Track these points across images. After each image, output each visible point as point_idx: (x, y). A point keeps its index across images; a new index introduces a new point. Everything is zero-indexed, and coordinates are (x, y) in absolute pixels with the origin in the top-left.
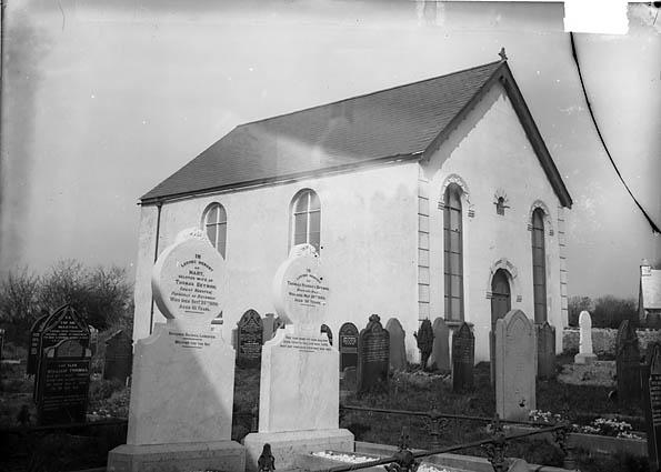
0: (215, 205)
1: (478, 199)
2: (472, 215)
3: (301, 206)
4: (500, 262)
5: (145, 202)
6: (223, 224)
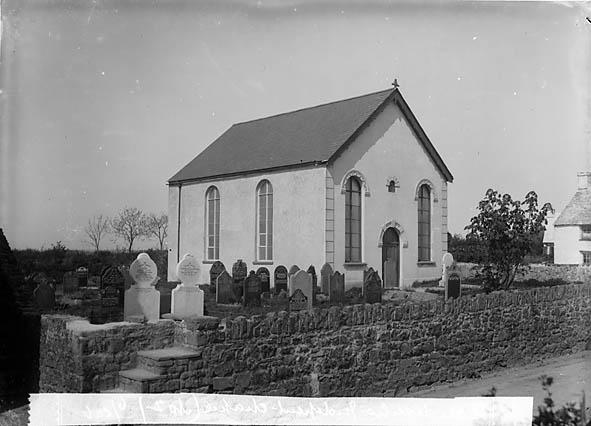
0: (213, 188)
1: (373, 184)
2: (367, 195)
3: (263, 190)
4: (390, 223)
5: (171, 183)
6: (271, 195)
